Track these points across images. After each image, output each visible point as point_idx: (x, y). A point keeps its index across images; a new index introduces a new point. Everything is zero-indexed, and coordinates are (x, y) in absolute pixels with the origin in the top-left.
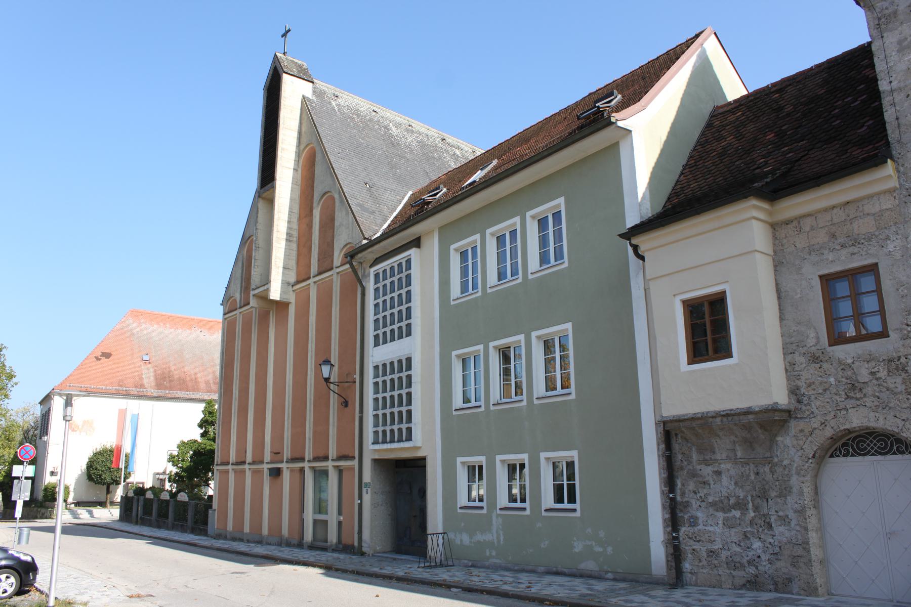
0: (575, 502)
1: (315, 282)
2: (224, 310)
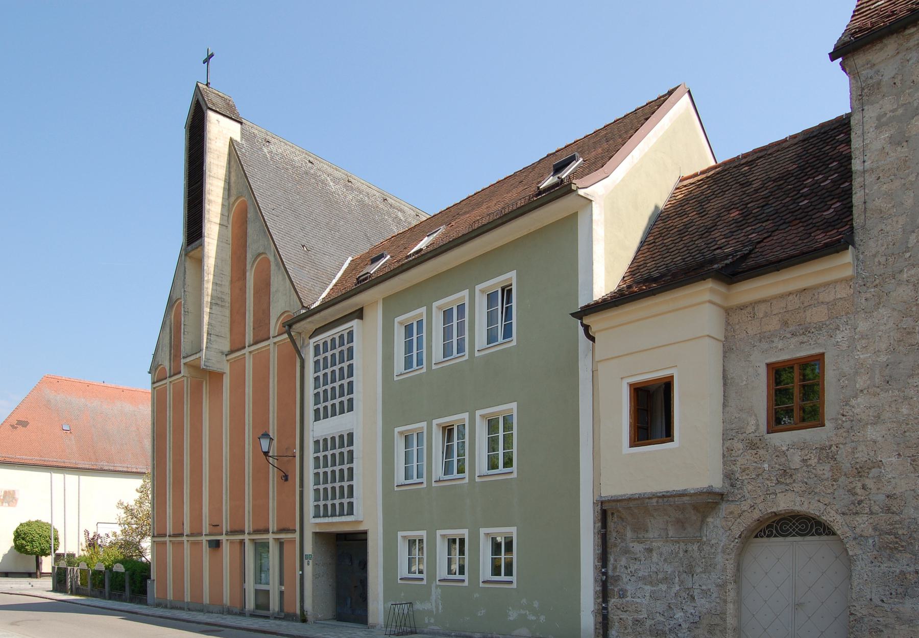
0: (463, 574)
2: (153, 378)
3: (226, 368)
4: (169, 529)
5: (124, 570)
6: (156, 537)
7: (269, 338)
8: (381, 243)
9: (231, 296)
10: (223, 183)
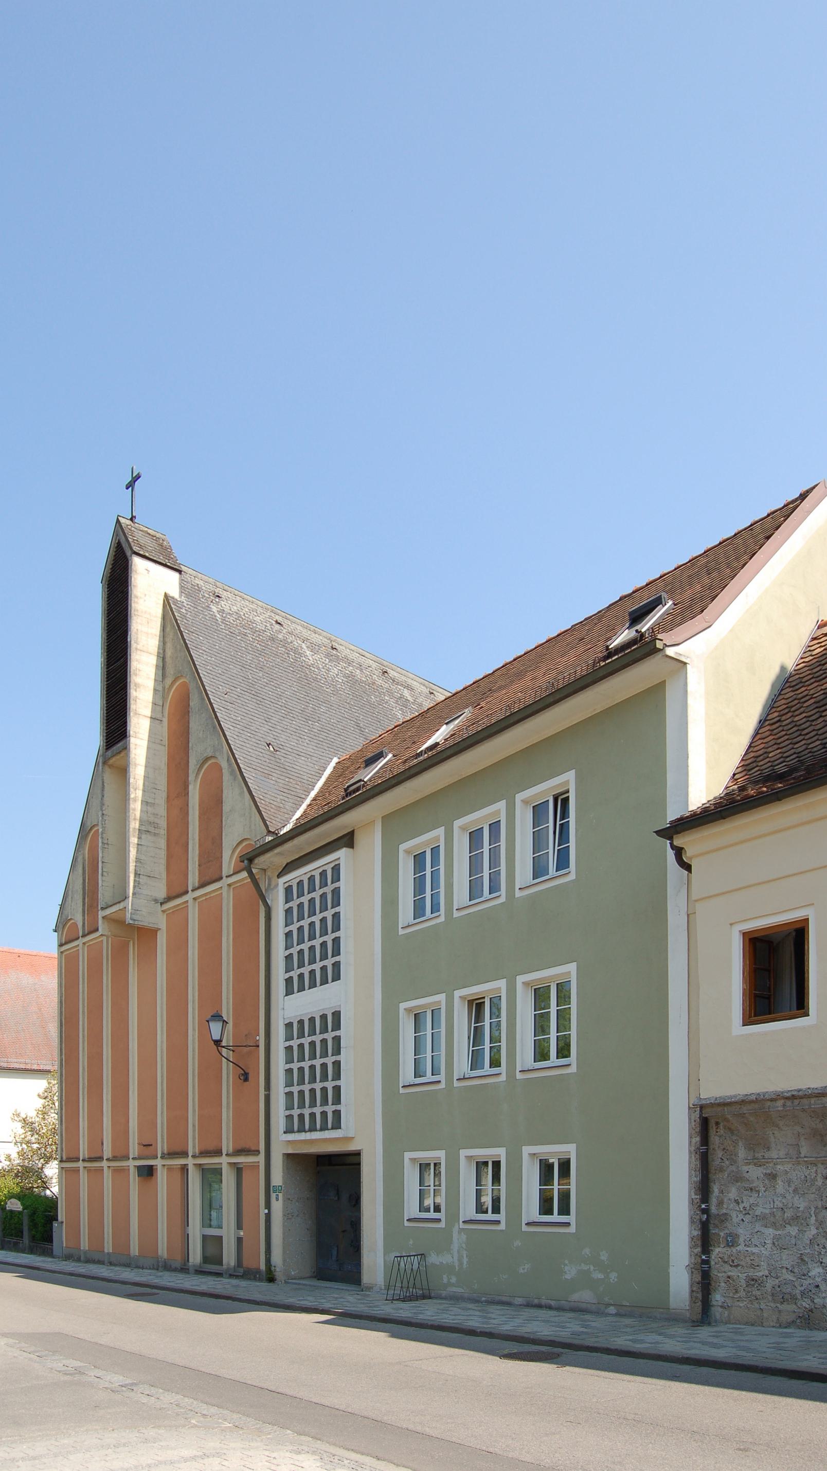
0: (568, 1213)
1: (195, 899)
2: (60, 939)
3: (160, 922)
4: (83, 1152)
5: (22, 1207)
7: (221, 878)
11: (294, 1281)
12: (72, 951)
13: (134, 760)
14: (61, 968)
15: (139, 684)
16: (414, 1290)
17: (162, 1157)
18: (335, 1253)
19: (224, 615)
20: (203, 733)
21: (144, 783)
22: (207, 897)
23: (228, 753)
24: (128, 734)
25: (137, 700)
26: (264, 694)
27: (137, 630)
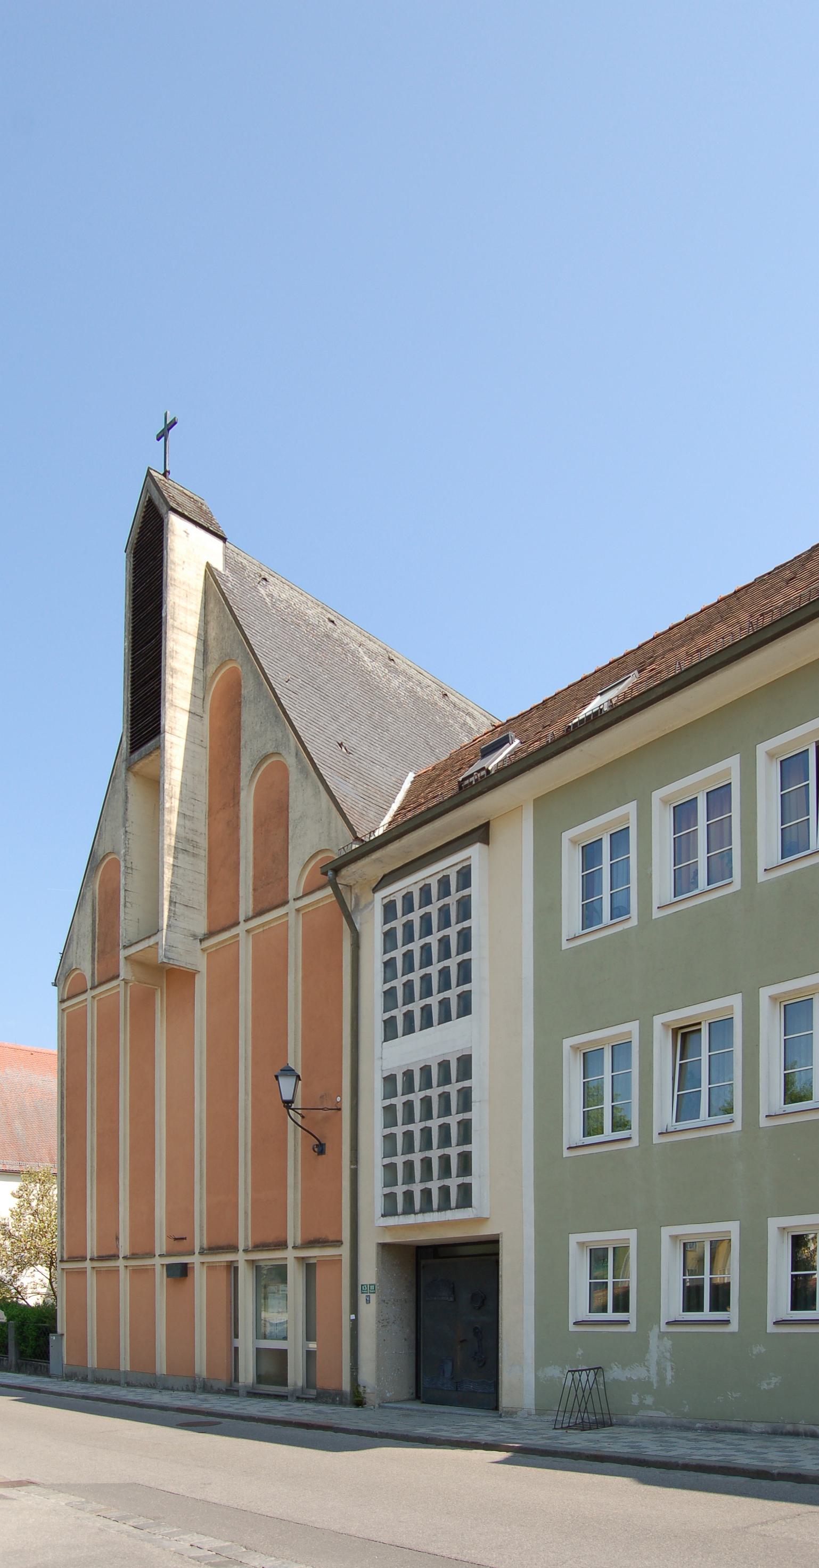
0: (626, 1309)
1: (248, 931)
2: (60, 993)
3: (200, 963)
4: (91, 1249)
5: (5, 1318)
6: (67, 1261)
7: (287, 902)
8: (474, 741)
9: (209, 838)
10: (195, 640)
11: (390, 1405)
12: (76, 1008)
13: (169, 762)
14: (62, 1028)
15: (176, 669)
16: (586, 1415)
17: (201, 1253)
18: (448, 1368)
19: (274, 600)
20: (261, 726)
21: (181, 791)
22: (265, 928)
23: (296, 747)
24: (162, 729)
25: (174, 688)
26: (328, 691)
27: (174, 603)
